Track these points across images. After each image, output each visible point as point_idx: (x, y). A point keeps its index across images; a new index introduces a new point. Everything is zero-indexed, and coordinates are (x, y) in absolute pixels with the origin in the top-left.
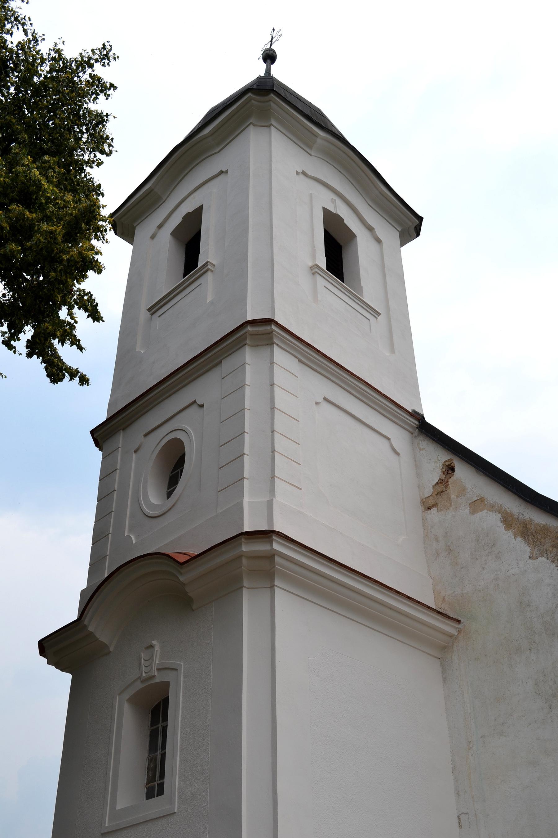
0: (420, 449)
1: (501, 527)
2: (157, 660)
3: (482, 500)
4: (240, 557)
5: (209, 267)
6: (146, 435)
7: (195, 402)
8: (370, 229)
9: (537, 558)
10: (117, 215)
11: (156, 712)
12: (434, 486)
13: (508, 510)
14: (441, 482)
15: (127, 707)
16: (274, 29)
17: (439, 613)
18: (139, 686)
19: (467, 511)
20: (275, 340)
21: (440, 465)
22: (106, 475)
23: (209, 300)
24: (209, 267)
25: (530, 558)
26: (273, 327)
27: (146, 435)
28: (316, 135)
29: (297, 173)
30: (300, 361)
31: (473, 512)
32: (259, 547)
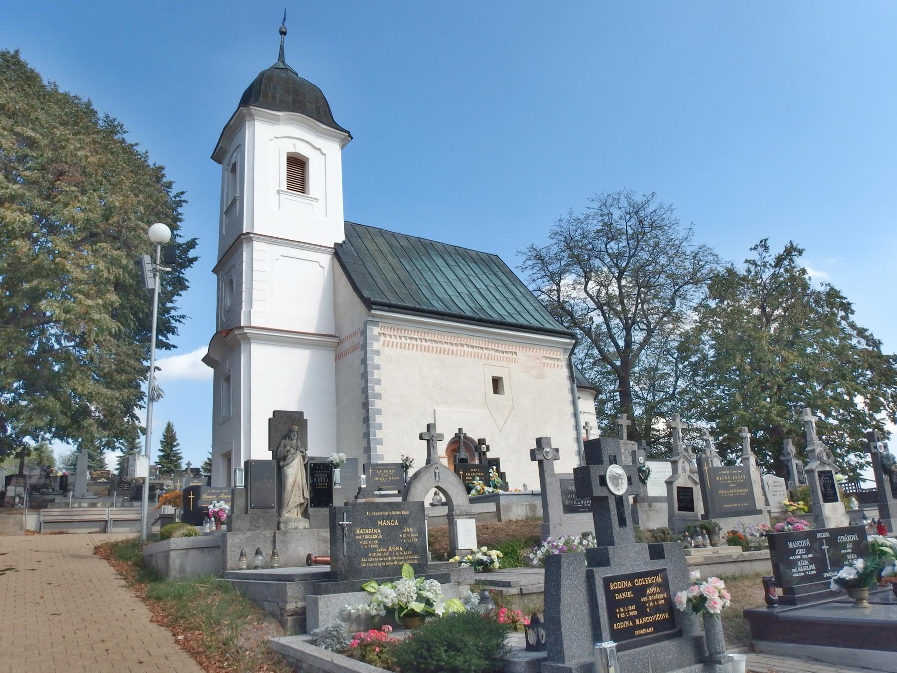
32: (240, 332)
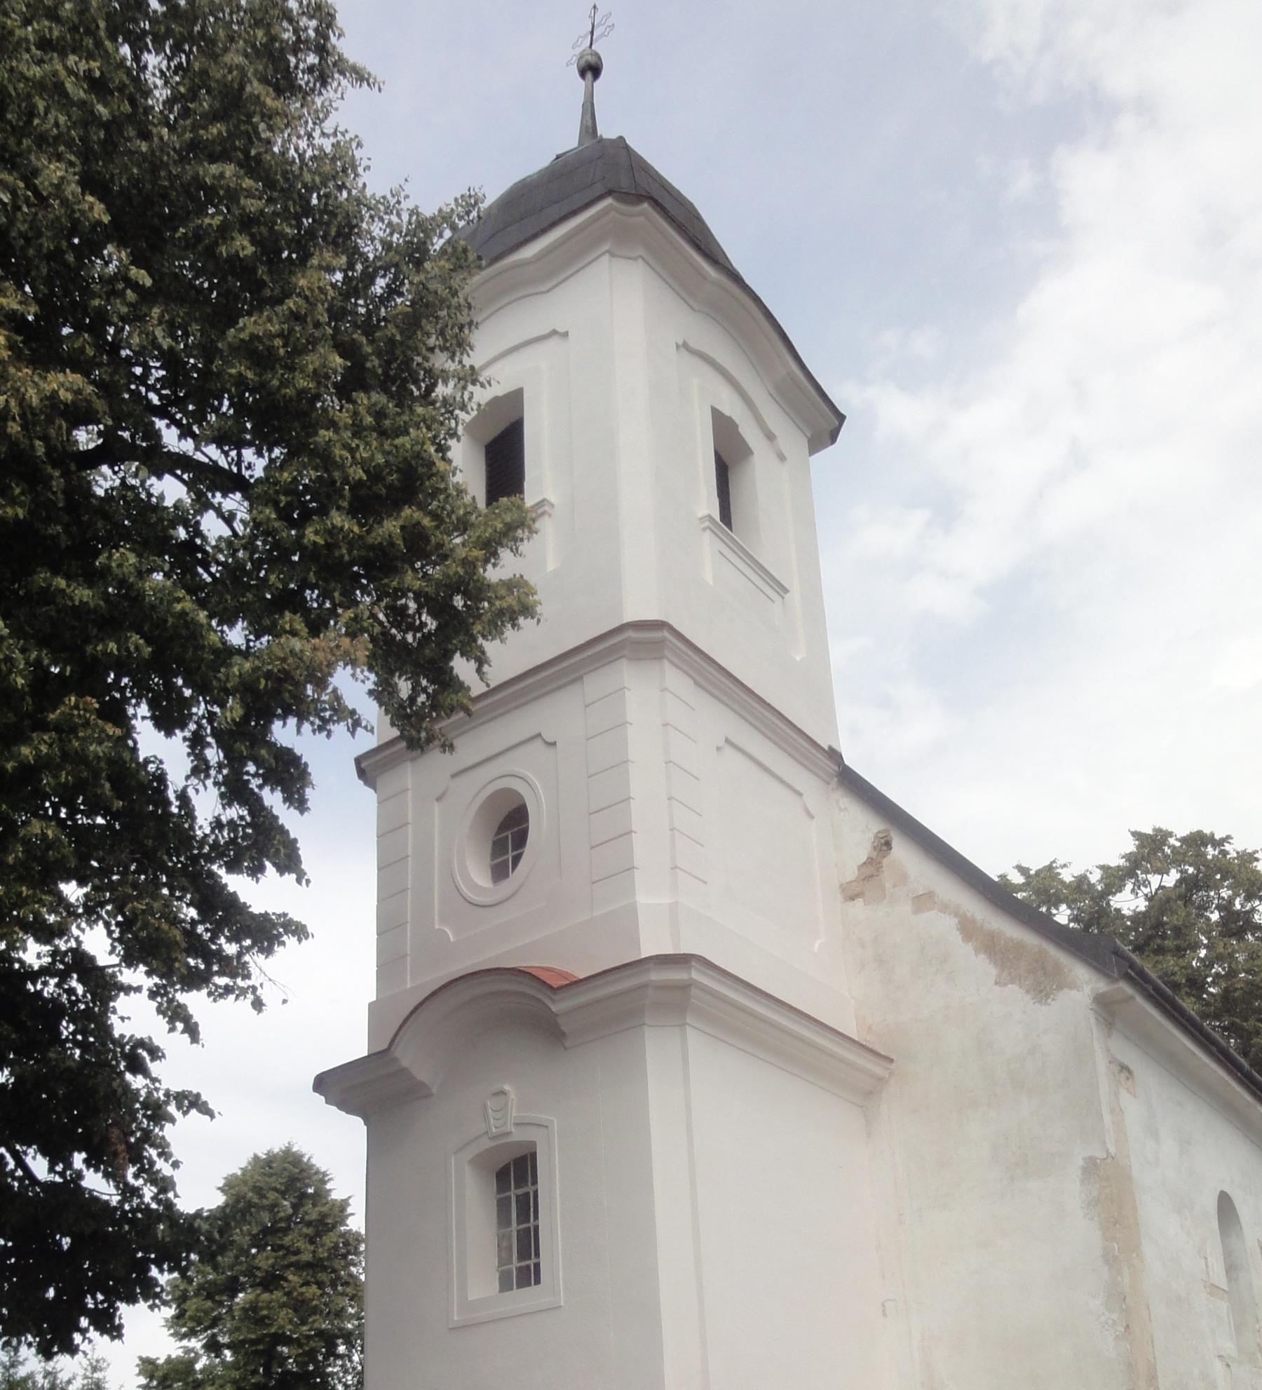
0: (840, 810)
1: (956, 937)
2: (514, 1113)
3: (930, 895)
4: (645, 986)
5: (546, 508)
6: (454, 776)
7: (539, 735)
8: (770, 437)
9: (1006, 985)
10: (780, 724)
11: (515, 1175)
12: (860, 867)
13: (969, 915)
14: (870, 861)
15: (467, 1169)
16: (595, 7)
17: (862, 1046)
18: (486, 1144)
19: (908, 908)
20: (667, 653)
21: (870, 836)
22: (389, 833)
23: (551, 567)
24: (546, 508)
25: (996, 983)
26: (666, 634)
27: (454, 776)
28: (704, 277)
29: (678, 346)
30: (696, 683)
31: (917, 910)
